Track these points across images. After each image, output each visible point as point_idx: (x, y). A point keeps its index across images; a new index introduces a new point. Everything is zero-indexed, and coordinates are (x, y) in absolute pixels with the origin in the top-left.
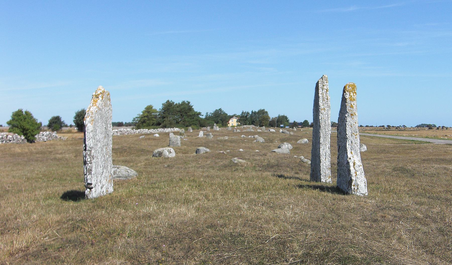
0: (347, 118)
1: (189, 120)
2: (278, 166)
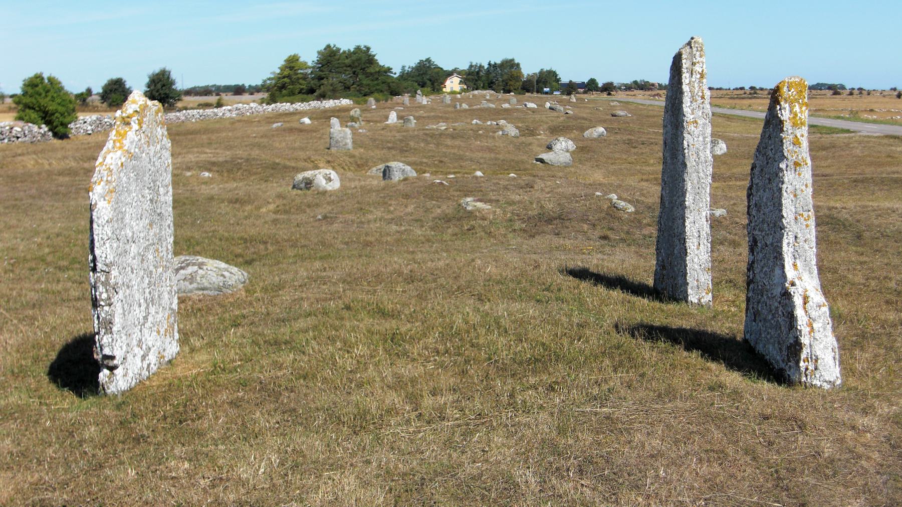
0: (785, 172)
1: (369, 82)
2: (563, 219)
